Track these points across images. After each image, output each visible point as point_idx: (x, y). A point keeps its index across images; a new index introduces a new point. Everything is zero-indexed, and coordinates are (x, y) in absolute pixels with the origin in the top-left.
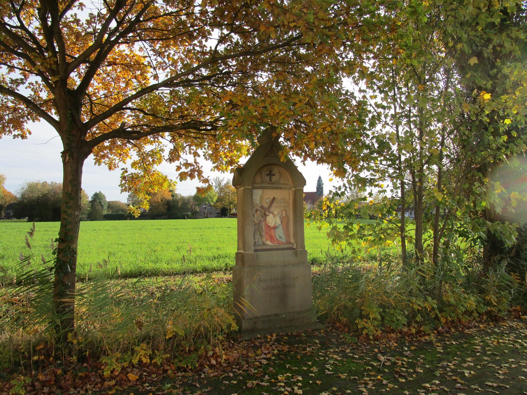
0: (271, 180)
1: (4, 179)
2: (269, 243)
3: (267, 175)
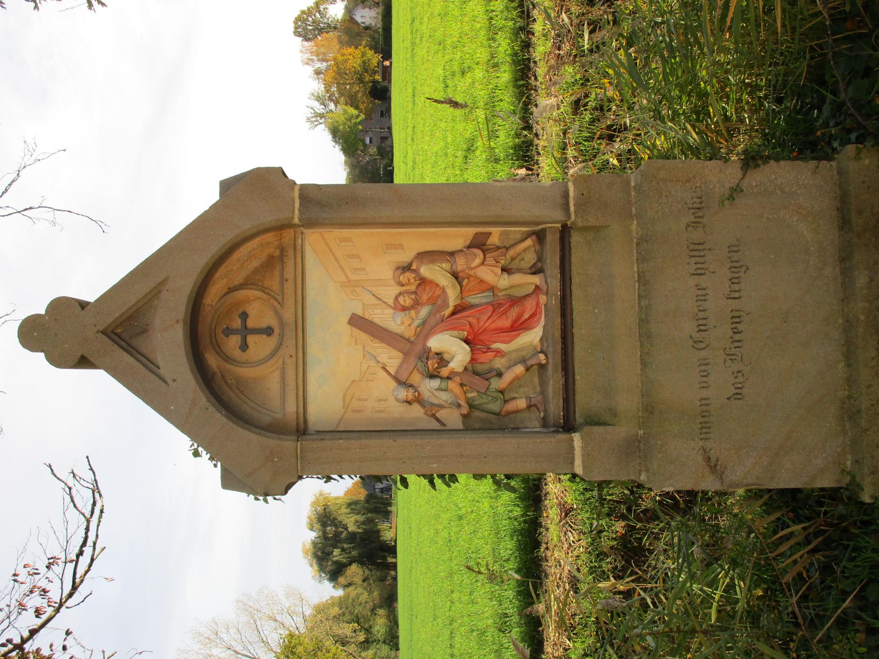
0: (268, 331)
1: (321, 494)
2: (533, 337)
3: (244, 346)
